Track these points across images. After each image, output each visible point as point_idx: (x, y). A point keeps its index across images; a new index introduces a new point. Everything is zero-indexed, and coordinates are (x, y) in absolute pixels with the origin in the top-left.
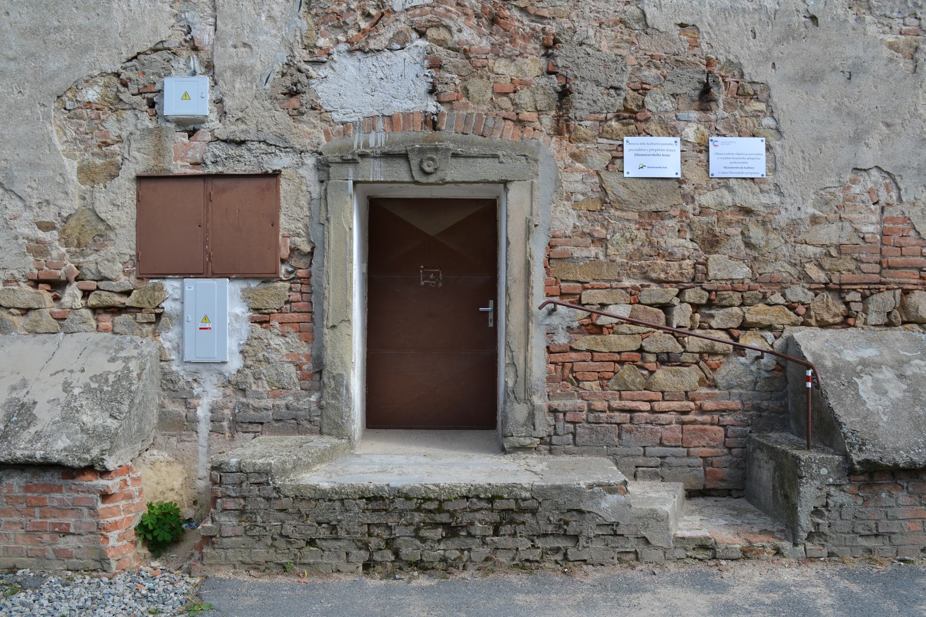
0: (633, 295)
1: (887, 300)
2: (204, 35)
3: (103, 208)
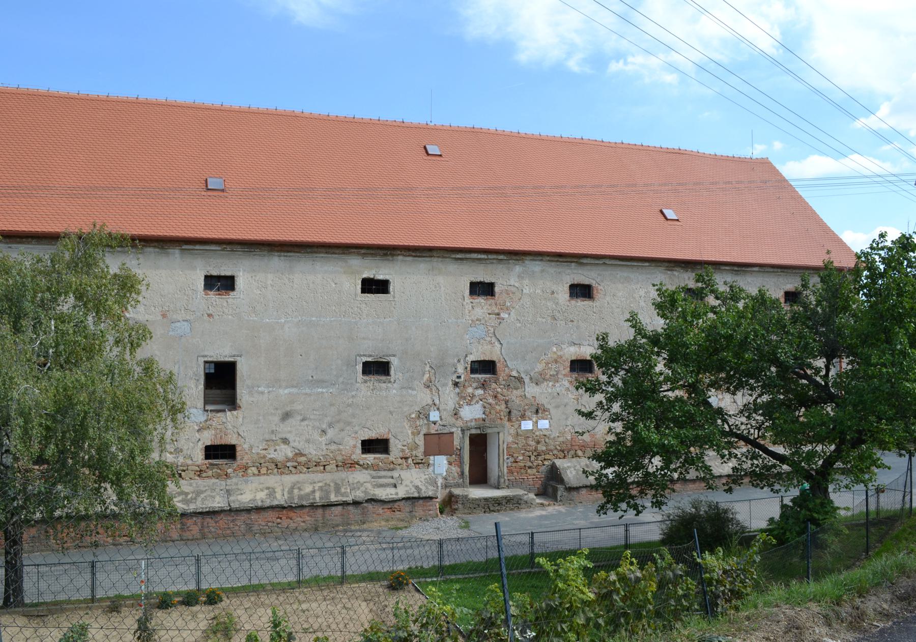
0: (523, 454)
1: (572, 452)
2: (437, 402)
3: (417, 441)
